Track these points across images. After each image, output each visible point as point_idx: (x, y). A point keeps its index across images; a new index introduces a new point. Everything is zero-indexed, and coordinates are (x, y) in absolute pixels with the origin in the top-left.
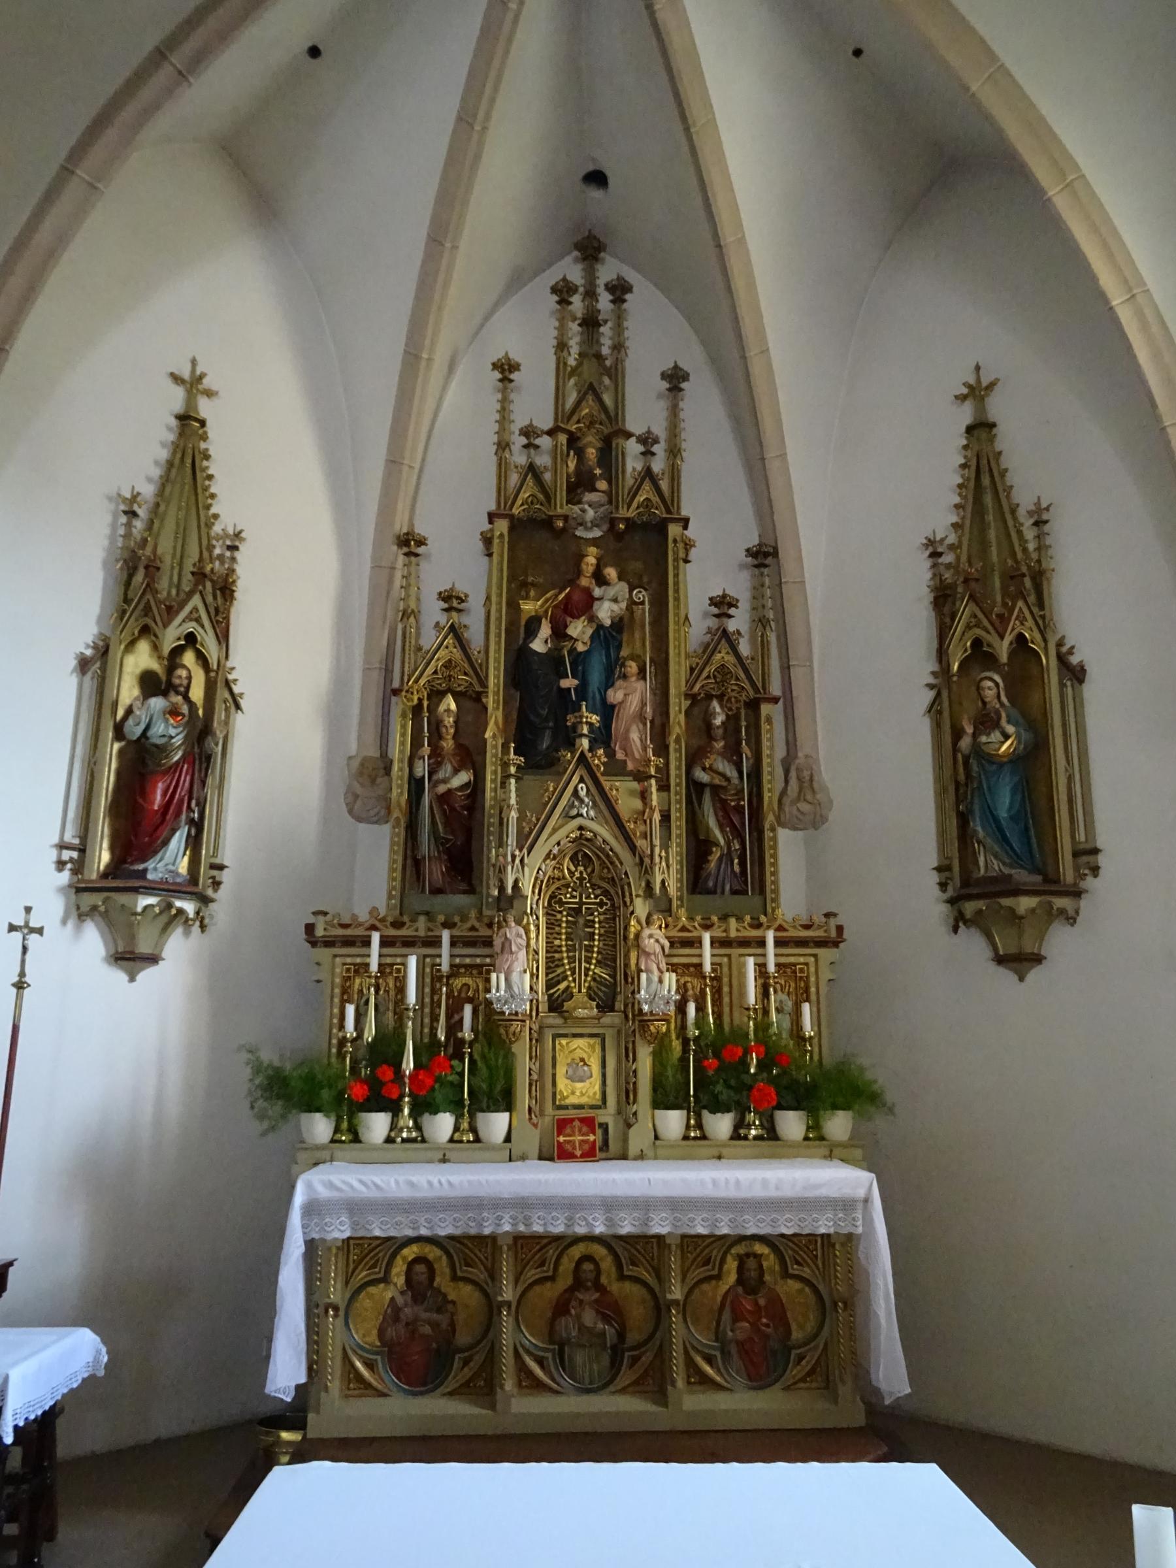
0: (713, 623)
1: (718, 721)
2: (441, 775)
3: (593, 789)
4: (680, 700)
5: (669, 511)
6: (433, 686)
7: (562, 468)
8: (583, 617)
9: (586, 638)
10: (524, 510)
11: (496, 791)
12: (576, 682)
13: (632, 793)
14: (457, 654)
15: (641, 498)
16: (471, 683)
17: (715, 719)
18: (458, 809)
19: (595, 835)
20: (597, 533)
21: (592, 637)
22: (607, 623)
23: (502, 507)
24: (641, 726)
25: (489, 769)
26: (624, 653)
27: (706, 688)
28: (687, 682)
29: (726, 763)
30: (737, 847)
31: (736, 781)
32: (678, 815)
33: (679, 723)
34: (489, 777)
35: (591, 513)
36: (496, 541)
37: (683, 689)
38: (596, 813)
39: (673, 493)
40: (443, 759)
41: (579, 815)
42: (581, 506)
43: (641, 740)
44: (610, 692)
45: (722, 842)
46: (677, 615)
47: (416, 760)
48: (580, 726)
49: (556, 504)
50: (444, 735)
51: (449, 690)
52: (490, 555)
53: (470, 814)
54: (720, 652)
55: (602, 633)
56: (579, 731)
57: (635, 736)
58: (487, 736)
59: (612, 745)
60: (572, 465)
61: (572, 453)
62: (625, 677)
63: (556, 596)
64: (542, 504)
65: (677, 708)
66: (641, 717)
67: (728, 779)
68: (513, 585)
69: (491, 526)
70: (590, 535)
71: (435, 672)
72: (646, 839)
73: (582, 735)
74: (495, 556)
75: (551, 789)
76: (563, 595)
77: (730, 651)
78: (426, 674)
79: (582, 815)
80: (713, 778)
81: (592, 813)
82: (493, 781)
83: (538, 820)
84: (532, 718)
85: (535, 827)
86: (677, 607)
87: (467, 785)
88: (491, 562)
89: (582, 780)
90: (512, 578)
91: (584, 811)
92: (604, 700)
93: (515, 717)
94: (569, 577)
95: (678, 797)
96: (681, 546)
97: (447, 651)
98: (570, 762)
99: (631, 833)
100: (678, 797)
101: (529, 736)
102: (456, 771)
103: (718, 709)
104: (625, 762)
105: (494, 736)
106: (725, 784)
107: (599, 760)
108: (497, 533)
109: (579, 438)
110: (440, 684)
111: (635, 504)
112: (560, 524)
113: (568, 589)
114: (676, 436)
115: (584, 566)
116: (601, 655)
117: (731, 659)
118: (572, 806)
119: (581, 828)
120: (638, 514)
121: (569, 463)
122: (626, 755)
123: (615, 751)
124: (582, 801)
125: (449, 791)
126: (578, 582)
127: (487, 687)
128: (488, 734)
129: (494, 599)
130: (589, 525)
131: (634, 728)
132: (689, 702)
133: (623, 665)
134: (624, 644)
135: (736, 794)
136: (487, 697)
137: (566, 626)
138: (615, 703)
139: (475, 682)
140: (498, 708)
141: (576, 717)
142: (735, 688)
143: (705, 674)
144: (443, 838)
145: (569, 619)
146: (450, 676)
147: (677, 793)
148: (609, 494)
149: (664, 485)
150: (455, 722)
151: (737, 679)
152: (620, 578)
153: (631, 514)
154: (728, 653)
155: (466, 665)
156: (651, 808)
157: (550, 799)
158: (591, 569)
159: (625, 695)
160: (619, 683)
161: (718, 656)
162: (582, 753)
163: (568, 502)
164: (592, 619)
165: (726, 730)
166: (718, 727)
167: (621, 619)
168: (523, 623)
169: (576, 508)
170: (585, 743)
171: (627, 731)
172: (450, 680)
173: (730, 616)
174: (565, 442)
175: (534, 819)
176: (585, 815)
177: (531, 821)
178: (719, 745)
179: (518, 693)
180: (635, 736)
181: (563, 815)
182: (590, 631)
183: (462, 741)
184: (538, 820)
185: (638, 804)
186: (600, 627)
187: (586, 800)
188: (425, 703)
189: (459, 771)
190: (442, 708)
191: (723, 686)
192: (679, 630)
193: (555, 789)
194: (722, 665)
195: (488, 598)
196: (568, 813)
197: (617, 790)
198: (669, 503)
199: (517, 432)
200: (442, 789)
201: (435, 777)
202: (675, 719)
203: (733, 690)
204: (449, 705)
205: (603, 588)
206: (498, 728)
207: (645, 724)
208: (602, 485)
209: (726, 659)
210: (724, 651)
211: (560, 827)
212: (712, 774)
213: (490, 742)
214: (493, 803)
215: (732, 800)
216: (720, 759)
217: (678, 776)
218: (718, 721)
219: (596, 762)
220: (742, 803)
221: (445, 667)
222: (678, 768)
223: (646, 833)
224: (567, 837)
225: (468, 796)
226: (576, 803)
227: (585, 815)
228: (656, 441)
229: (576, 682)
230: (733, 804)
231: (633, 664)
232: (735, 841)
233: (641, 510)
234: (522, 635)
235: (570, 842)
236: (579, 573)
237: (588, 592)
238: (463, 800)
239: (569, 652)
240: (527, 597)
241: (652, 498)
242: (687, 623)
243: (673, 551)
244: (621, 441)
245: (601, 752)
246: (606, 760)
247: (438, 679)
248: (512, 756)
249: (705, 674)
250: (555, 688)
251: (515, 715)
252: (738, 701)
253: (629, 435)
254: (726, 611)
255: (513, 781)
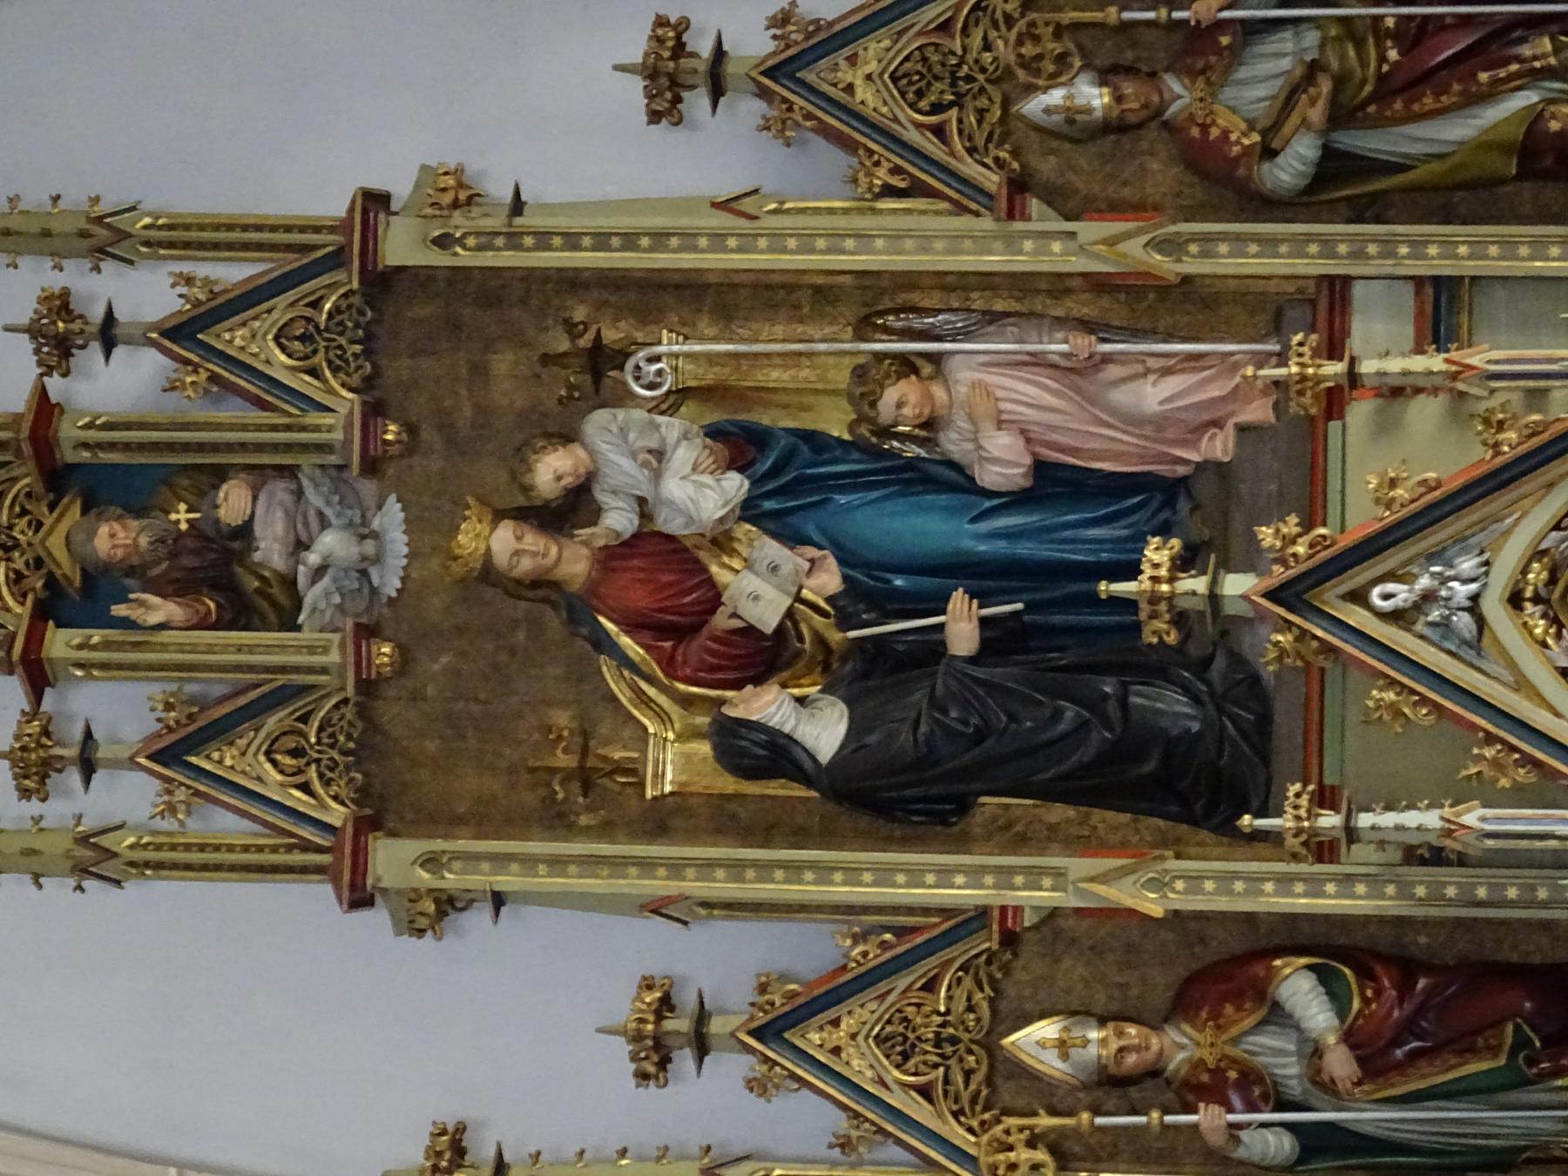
0: (746, 109)
1: (1094, 97)
2: (1289, 1070)
3: (1391, 560)
4: (1028, 235)
5: (337, 259)
6: (974, 1100)
7: (164, 647)
8: (714, 569)
9: (790, 560)
10: (327, 783)
11: (1349, 879)
12: (958, 599)
13: (1385, 427)
14: (860, 1014)
15: (279, 363)
16: (964, 968)
17: (1089, 110)
18: (1409, 1007)
19: (1539, 554)
20: (391, 519)
21: (794, 539)
22: (735, 485)
23: (325, 859)
24: (1113, 371)
25: (1272, 902)
26: (835, 422)
27: (980, 141)
28: (961, 209)
29: (1242, 73)
30: (1546, 44)
31: (1312, 38)
32: (1433, 250)
33: (1111, 242)
34: (1300, 902)
35: (332, 543)
36: (451, 880)
37: (987, 223)
38: (1465, 551)
39: (260, 247)
40: (1234, 1061)
41: (1474, 605)
42: (302, 580)
43: (1167, 372)
44: (990, 477)
45: (1528, 98)
46: (718, 240)
47: (1240, 1153)
48: (1184, 604)
49: (310, 670)
50: (1150, 1056)
51: (990, 1045)
52: (498, 900)
53: (1428, 969)
54: (850, 89)
55: (769, 505)
56: (1200, 605)
57: (1153, 395)
58: (1157, 911)
59: (1181, 470)
60: (160, 609)
61: (119, 610)
62: (931, 425)
63: (625, 661)
64: (304, 719)
65: (1056, 247)
66: (1075, 372)
67: (1313, 70)
68: (584, 820)
69: (379, 899)
70: (398, 542)
71: (925, 1092)
72: (1546, 390)
73: (1214, 598)
74: (506, 881)
75: (1390, 696)
76: (625, 641)
77: (846, 52)
78: (933, 1124)
79: (1475, 598)
80: (1305, 123)
81: (1467, 565)
82: (1315, 886)
83: (1490, 739)
84: (1086, 753)
85: (1514, 749)
86: (689, 239)
87: (1325, 977)
88: (527, 898)
89: (1359, 597)
90: (557, 821)
91: (1462, 591)
92: (1017, 500)
93: (1071, 812)
94: (554, 621)
95: (1372, 249)
96: (459, 223)
97: (849, 1052)
98: (1303, 635)
99: (1535, 442)
100: (1372, 249)
101: (1149, 767)
102: (1277, 1015)
103: (1056, 97)
104: (1242, 429)
105: (1158, 885)
106: (1325, 86)
107: (1293, 542)
108: (424, 877)
109: (51, 582)
110: (968, 1074)
111: (304, 384)
112: (385, 651)
113: (602, 620)
114: (46, 233)
115: (526, 565)
116: (849, 509)
117: (875, 52)
118: (1444, 625)
119: (1515, 600)
120: (335, 370)
121: (154, 618)
122: (1217, 424)
123: (1201, 467)
124: (1428, 597)
125: (1349, 1038)
126: (575, 587)
127: (983, 912)
128: (1152, 904)
129: (659, 886)
130: (369, 547)
131: (1121, 396)
132: (1035, 205)
133: (886, 432)
134: (807, 422)
135: (1360, 45)
136: (1018, 910)
137: (750, 631)
138: (1028, 460)
139: (960, 953)
140: (1059, 873)
141: (1154, 616)
142: (976, 40)
143: (931, 146)
144: (1513, 1054)
145: (721, 621)
146: (938, 1043)
147: (1358, 255)
148: (260, 476)
149: (233, 273)
150: (1102, 1021)
151: (945, 27)
152: (567, 436)
153: (346, 401)
154: (852, 60)
155: (902, 983)
156: (1454, 376)
157: (1424, 700)
158: (533, 540)
159: (1000, 424)
160: (953, 443)
161: (865, 95)
162: (1273, 595)
163: (289, 623)
164: (721, 542)
165: (1130, 71)
166: (1119, 98)
167: (714, 433)
168: (729, 784)
169: (312, 596)
170: (1236, 585)
171: (1134, 421)
172: (954, 1041)
173: (719, 54)
174: (76, 635)
175: (1489, 752)
176: (1474, 587)
177: (1495, 763)
178: (1179, 93)
179: (984, 799)
180: (1153, 395)
181: (1469, 654)
182: (771, 549)
183: (1161, 998)
184: (1490, 739)
185: (1425, 412)
186: (749, 511)
187: (1424, 582)
188: (1045, 1121)
189: (1276, 1006)
190: (1052, 1065)
191: (969, 79)
192: (776, 236)
193: (1392, 683)
194: (894, 78)
195: (657, 908)
196: (1465, 642)
197: (1393, 483)
198: (293, 262)
199: (34, 807)
200: (1340, 1064)
201: (1295, 1088)
202: (1098, 257)
203: (987, 47)
204: (1042, 1044)
205: (602, 497)
206: (1123, 872)
207: (1107, 359)
208: (233, 502)
209: (873, 67)
210: (846, 75)
211: (1512, 665)
212: (1287, 129)
213: (1180, 899)
214: (1390, 890)
215: (1382, 59)
216: (1228, 93)
217: (1298, 245)
218: (1094, 97)
219: (1300, 549)
220: (1390, 22)
221: (906, 1056)
222: (1269, 244)
223: (1530, 392)
224: (1544, 645)
225: (1365, 974)
226: (1435, 615)
227: (1474, 587)
228: (60, 304)
229: (958, 599)
230: (1393, 55)
231: (891, 395)
232: (1526, 51)
233: (319, 359)
234: (777, 788)
235: (1559, 636)
236: (542, 586)
237: (614, 555)
238: (1378, 993)
239: (845, 622)
240: (633, 771)
241: (280, 316)
242: (747, 205)
243: (480, 248)
244: (68, 431)
245: (1266, 535)
246: (1293, 519)
247: (946, 1081)
248: (1285, 822)
249: (931, 146)
250: (980, 673)
251: (1059, 813)
252: (1031, 35)
253: (45, 409)
254: (702, 67)
255: (1364, 820)
